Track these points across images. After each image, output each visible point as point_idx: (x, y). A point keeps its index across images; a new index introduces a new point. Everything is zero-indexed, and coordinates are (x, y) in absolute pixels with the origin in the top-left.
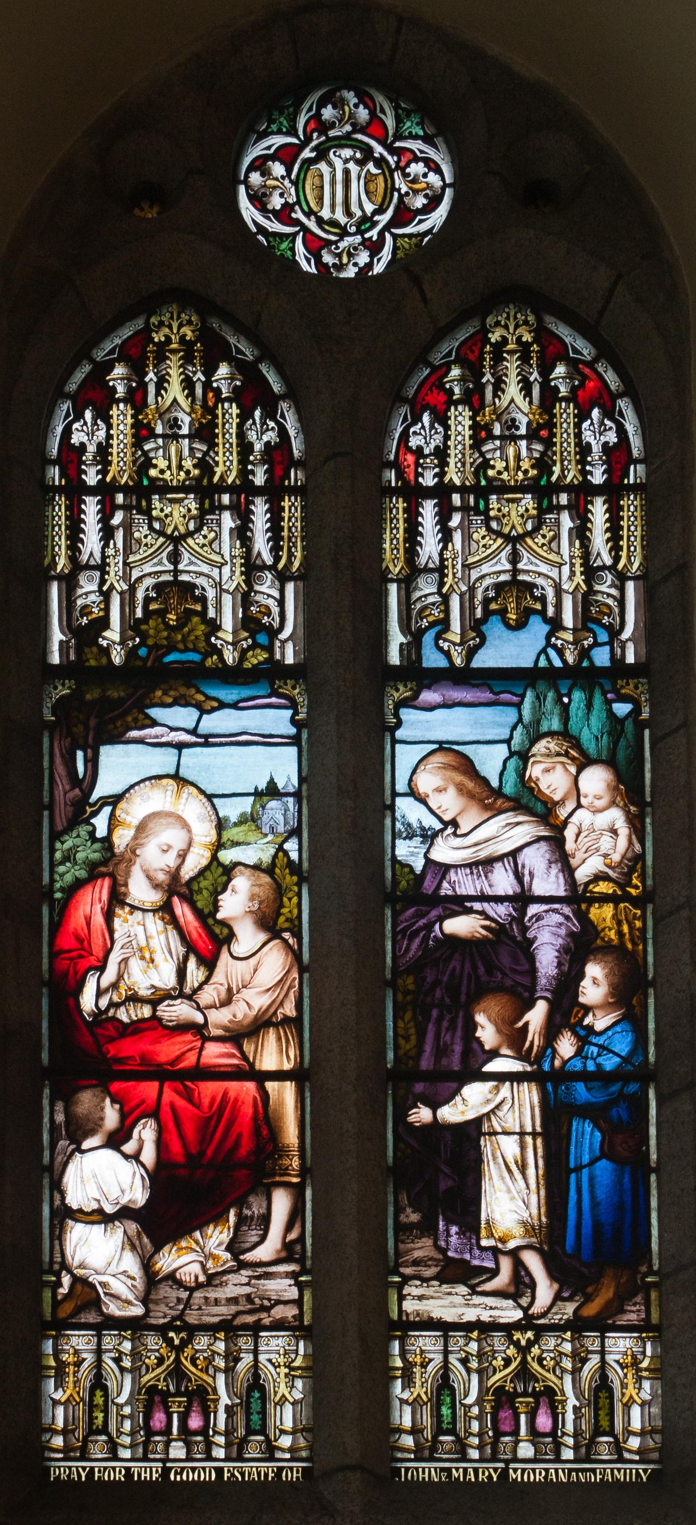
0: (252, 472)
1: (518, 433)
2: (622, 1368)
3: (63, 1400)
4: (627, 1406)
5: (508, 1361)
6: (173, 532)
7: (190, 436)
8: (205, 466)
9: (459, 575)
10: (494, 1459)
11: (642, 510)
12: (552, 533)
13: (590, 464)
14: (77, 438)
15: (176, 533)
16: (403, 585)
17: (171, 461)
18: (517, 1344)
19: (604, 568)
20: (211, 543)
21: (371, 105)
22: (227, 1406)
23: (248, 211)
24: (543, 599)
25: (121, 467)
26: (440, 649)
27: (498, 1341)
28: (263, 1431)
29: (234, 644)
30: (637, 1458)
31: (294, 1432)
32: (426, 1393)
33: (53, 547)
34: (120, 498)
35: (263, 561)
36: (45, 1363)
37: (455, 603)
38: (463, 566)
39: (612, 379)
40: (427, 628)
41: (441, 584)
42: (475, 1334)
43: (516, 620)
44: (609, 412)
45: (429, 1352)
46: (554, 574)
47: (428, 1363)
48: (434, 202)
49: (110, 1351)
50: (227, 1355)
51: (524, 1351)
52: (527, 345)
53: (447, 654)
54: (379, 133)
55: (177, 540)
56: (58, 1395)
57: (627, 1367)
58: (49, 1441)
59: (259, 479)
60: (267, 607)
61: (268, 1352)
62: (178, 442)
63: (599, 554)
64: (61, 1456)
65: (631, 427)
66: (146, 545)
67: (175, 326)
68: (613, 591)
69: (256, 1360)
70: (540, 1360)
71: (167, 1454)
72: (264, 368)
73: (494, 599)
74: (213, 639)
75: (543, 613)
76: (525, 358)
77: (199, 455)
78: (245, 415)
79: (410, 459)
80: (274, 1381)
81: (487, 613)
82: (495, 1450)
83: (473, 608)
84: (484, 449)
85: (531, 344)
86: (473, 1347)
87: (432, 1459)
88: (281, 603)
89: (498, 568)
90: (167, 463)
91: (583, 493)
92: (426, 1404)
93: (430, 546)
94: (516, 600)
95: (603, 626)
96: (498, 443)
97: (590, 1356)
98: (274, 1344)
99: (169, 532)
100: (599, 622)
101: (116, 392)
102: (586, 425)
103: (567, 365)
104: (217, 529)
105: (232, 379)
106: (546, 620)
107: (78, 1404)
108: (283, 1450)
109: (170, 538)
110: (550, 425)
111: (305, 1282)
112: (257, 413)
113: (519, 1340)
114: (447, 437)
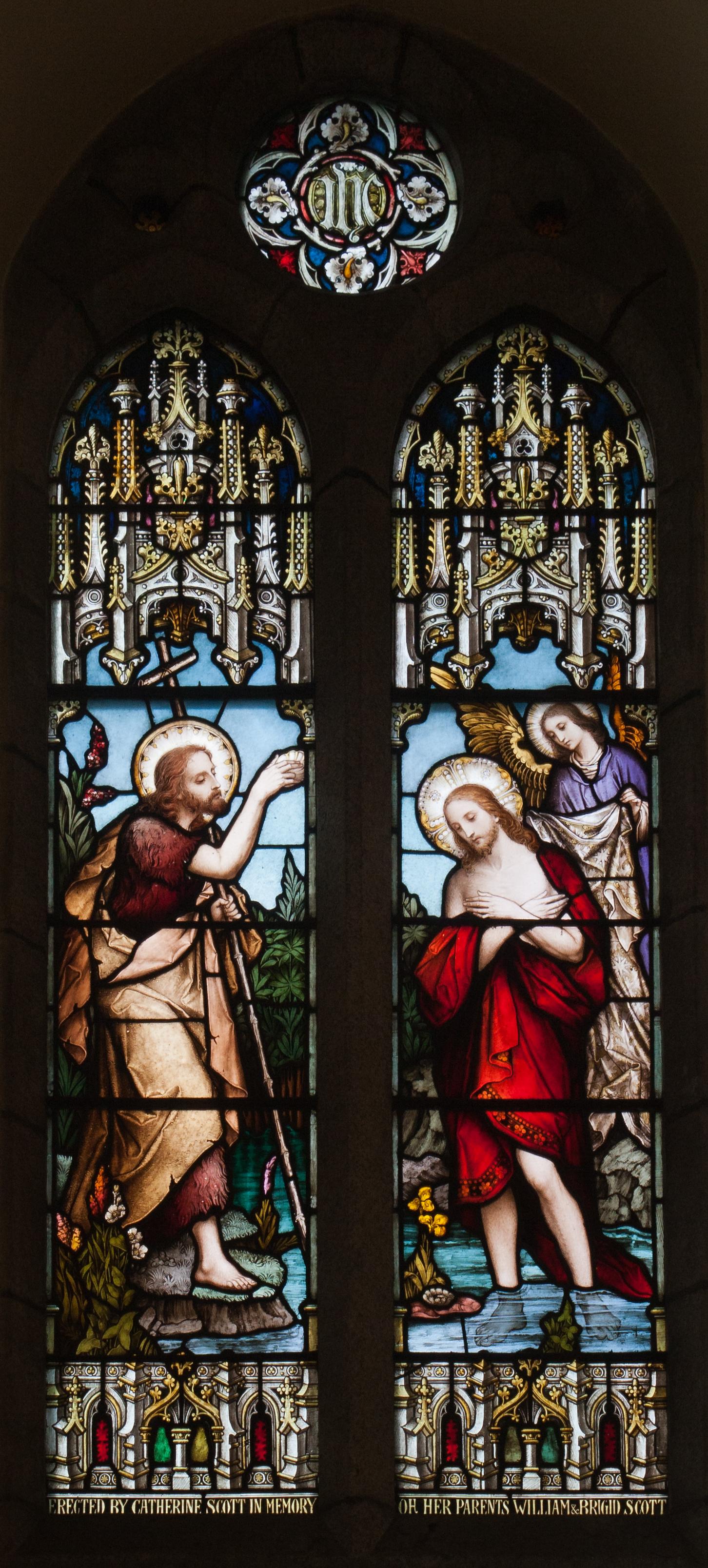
0: (258, 491)
1: (530, 455)
2: (628, 1399)
3: (66, 1430)
4: (633, 1436)
5: (513, 1392)
6: (178, 548)
7: (539, 458)
9: (469, 596)
10: (499, 1491)
12: (217, 550)
13: (601, 484)
14: (79, 455)
15: (525, 555)
16: (412, 608)
17: (522, 484)
19: (271, 586)
20: (561, 564)
21: (370, 118)
22: (231, 1436)
23: (253, 228)
24: (208, 617)
25: (128, 483)
26: (104, 666)
27: (506, 1372)
28: (268, 1461)
29: (472, 667)
30: (643, 1488)
31: (648, 1465)
32: (82, 1423)
33: (57, 566)
34: (124, 517)
35: (614, 585)
36: (50, 1393)
37: (119, 618)
38: (129, 580)
39: (426, 399)
40: (91, 646)
41: (451, 605)
42: (481, 1365)
43: (181, 637)
44: (274, 431)
45: (87, 1381)
46: (565, 597)
47: (433, 1395)
49: (462, 1382)
50: (231, 1384)
52: (539, 366)
54: (380, 146)
55: (526, 563)
56: (60, 1426)
58: (53, 1472)
59: (264, 497)
60: (618, 631)
61: (270, 1381)
62: (527, 465)
63: (265, 572)
64: (643, 1488)
65: (642, 448)
66: (150, 561)
67: (522, 348)
68: (278, 611)
69: (260, 1390)
70: (546, 1393)
71: (521, 1484)
72: (612, 388)
73: (159, 616)
74: (563, 663)
75: (553, 636)
76: (192, 375)
77: (203, 471)
78: (593, 437)
79: (421, 479)
80: (628, 1413)
81: (497, 636)
82: (500, 1483)
83: (138, 626)
84: (151, 464)
85: (543, 365)
86: (131, 1376)
87: (87, 1490)
88: (632, 627)
89: (509, 590)
90: (514, 485)
91: (249, 511)
92: (82, 1434)
93: (440, 567)
94: (182, 620)
95: (269, 645)
96: (165, 458)
97: (596, 1386)
98: (628, 1377)
99: (518, 553)
100: (264, 641)
101: (120, 409)
102: (597, 446)
103: (235, 382)
104: (222, 545)
105: (477, 401)
106: (556, 644)
107: (431, 1435)
108: (287, 1480)
109: (519, 560)
110: (561, 447)
111: (657, 1314)
112: (606, 435)
113: (524, 1369)
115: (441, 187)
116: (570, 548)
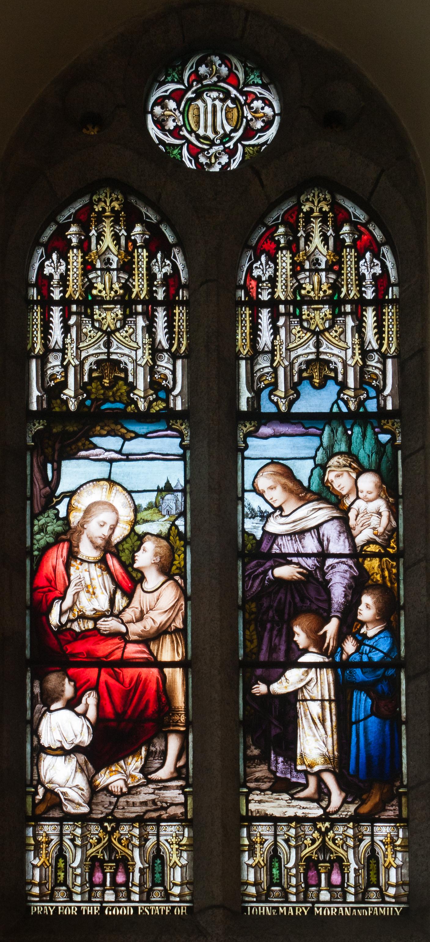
0: (156, 292)
1: (320, 267)
2: (385, 845)
3: (39, 865)
4: (387, 869)
5: (314, 841)
6: (107, 328)
7: (117, 270)
9: (284, 355)
12: (341, 329)
13: (364, 286)
15: (109, 329)
16: (249, 362)
17: (105, 285)
19: (373, 351)
20: (130, 336)
21: (229, 65)
22: (140, 868)
23: (153, 131)
24: (335, 370)
25: (75, 289)
26: (272, 401)
27: (308, 828)
28: (162, 884)
29: (145, 398)
30: (393, 900)
31: (181, 885)
32: (263, 860)
33: (33, 338)
34: (74, 308)
35: (163, 347)
36: (28, 842)
37: (281, 372)
38: (286, 349)
40: (264, 388)
41: (273, 361)
42: (293, 824)
43: (319, 383)
44: (376, 255)
45: (265, 835)
47: (264, 842)
49: (68, 834)
50: (140, 837)
52: (326, 213)
53: (276, 404)
54: (234, 82)
55: (109, 334)
56: (36, 862)
57: (387, 844)
58: (30, 890)
59: (160, 296)
60: (165, 375)
61: (165, 835)
62: (110, 273)
63: (370, 342)
64: (37, 899)
65: (390, 264)
66: (90, 337)
67: (108, 201)
68: (379, 365)
69: (158, 840)
70: (334, 840)
71: (103, 898)
72: (163, 227)
73: (305, 370)
74: (132, 395)
75: (335, 379)
76: (324, 221)
77: (123, 281)
78: (151, 257)
79: (254, 283)
80: (170, 853)
81: (301, 379)
82: (306, 896)
83: (292, 376)
84: (299, 277)
85: (328, 213)
86: (293, 832)
88: (174, 372)
89: (308, 351)
90: (103, 286)
91: (360, 304)
92: (263, 867)
94: (319, 371)
95: (373, 387)
96: (307, 273)
97: (364, 838)
98: (170, 830)
99: (104, 328)
100: (370, 384)
101: (72, 242)
102: (362, 262)
103: (350, 225)
104: (134, 327)
105: (144, 234)
106: (337, 383)
107: (48, 867)
108: (175, 896)
109: (105, 332)
110: (340, 262)
111: (189, 792)
112: (159, 255)
113: (320, 827)
114: (67, 270)
115: (271, 105)
116: (345, 325)
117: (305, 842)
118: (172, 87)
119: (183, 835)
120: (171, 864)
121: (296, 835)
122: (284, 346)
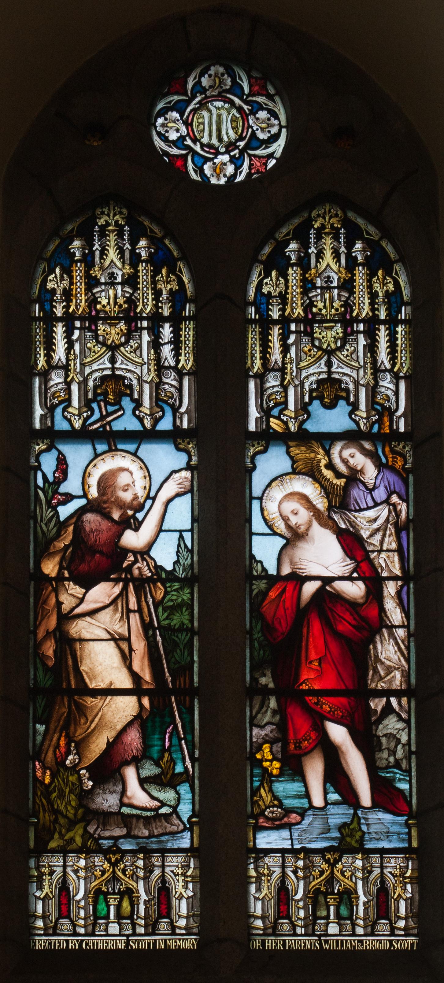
0: (162, 308)
1: (332, 285)
2: (394, 877)
3: (42, 897)
4: (397, 901)
5: (322, 873)
6: (111, 343)
7: (338, 287)
8: (131, 302)
9: (294, 374)
10: (313, 934)
11: (194, 331)
12: (136, 345)
13: (377, 304)
14: (50, 285)
15: (329, 348)
16: (258, 381)
17: (327, 303)
18: (327, 861)
19: (170, 367)
20: (352, 354)
21: (232, 74)
22: (145, 900)
23: (159, 143)
24: (130, 387)
25: (81, 303)
26: (65, 418)
27: (317, 860)
28: (168, 916)
29: (296, 418)
30: (403, 933)
31: (406, 918)
32: (51, 892)
33: (36, 355)
34: (78, 324)
35: (385, 367)
36: (31, 873)
37: (75, 387)
38: (81, 364)
40: (57, 405)
41: (283, 379)
42: (302, 856)
43: (114, 399)
44: (172, 270)
45: (55, 866)
47: (272, 874)
48: (275, 138)
49: (290, 867)
50: (145, 868)
51: (332, 865)
52: (338, 229)
53: (286, 423)
55: (330, 353)
56: (38, 894)
57: (396, 876)
58: (33, 923)
59: (166, 312)
60: (387, 396)
61: (169, 866)
62: (330, 291)
63: (166, 359)
64: (403, 933)
65: (403, 281)
66: (94, 352)
67: (327, 218)
68: (174, 383)
69: (163, 872)
70: (342, 873)
71: (327, 930)
72: (384, 243)
73: (100, 386)
74: (353, 416)
75: (347, 399)
76: (120, 235)
77: (128, 295)
78: (372, 274)
79: (264, 300)
81: (311, 399)
82: (314, 930)
83: (86, 392)
84: (94, 291)
85: (340, 229)
86: (82, 863)
87: (55, 934)
88: (397, 393)
89: (319, 370)
90: (323, 304)
91: (156, 320)
92: (52, 899)
94: (114, 388)
95: (169, 404)
96: (103, 287)
97: (374, 869)
98: (394, 863)
99: (325, 346)
100: (166, 402)
101: (75, 256)
102: (374, 279)
103: (147, 239)
104: (139, 342)
105: (299, 251)
106: (349, 404)
107: (270, 900)
108: (180, 928)
109: (325, 351)
110: (352, 280)
111: (412, 824)
112: (380, 272)
113: (329, 858)
114: (71, 283)
117: (313, 873)
118: (176, 98)
119: (407, 867)
120: (395, 897)
121: (363, 866)
122: (78, 360)
